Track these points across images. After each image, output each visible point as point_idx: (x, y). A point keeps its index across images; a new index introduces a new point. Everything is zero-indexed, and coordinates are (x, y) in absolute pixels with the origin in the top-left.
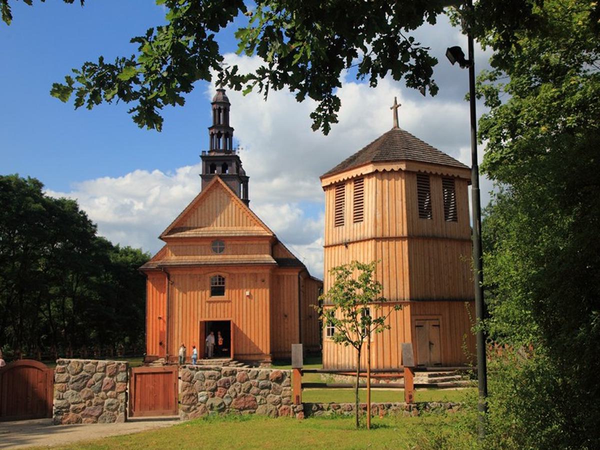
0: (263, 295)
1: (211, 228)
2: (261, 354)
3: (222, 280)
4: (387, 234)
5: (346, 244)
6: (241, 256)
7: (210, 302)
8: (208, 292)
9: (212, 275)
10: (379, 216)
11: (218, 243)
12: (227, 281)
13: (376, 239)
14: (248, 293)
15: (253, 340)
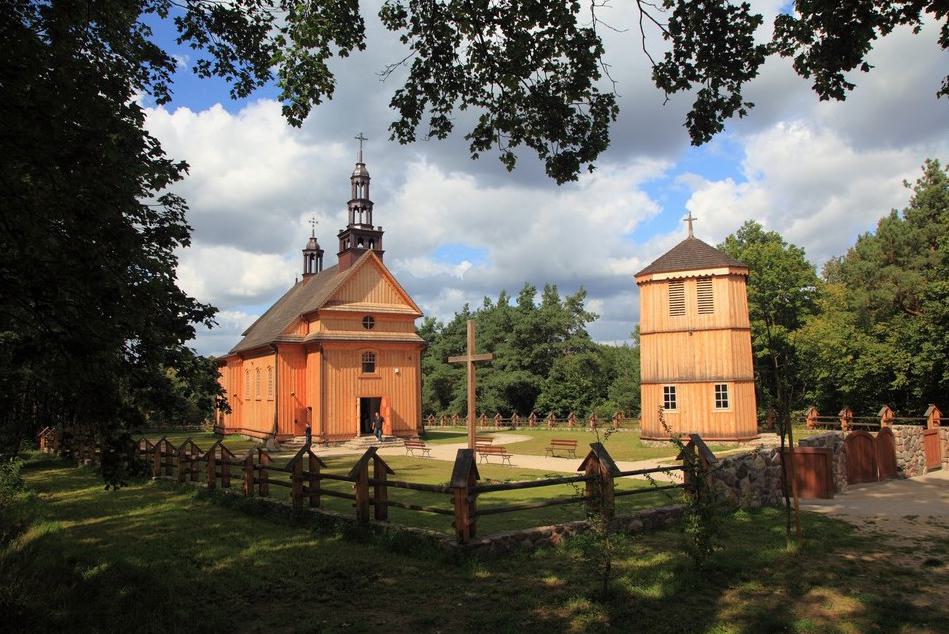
0: (410, 373)
1: (363, 303)
2: (410, 430)
3: (372, 356)
4: (738, 326)
5: (691, 332)
6: (391, 334)
7: (362, 379)
8: (360, 369)
9: (364, 351)
10: (732, 311)
11: (369, 320)
12: (378, 359)
13: (733, 329)
14: (397, 370)
15: (402, 417)
